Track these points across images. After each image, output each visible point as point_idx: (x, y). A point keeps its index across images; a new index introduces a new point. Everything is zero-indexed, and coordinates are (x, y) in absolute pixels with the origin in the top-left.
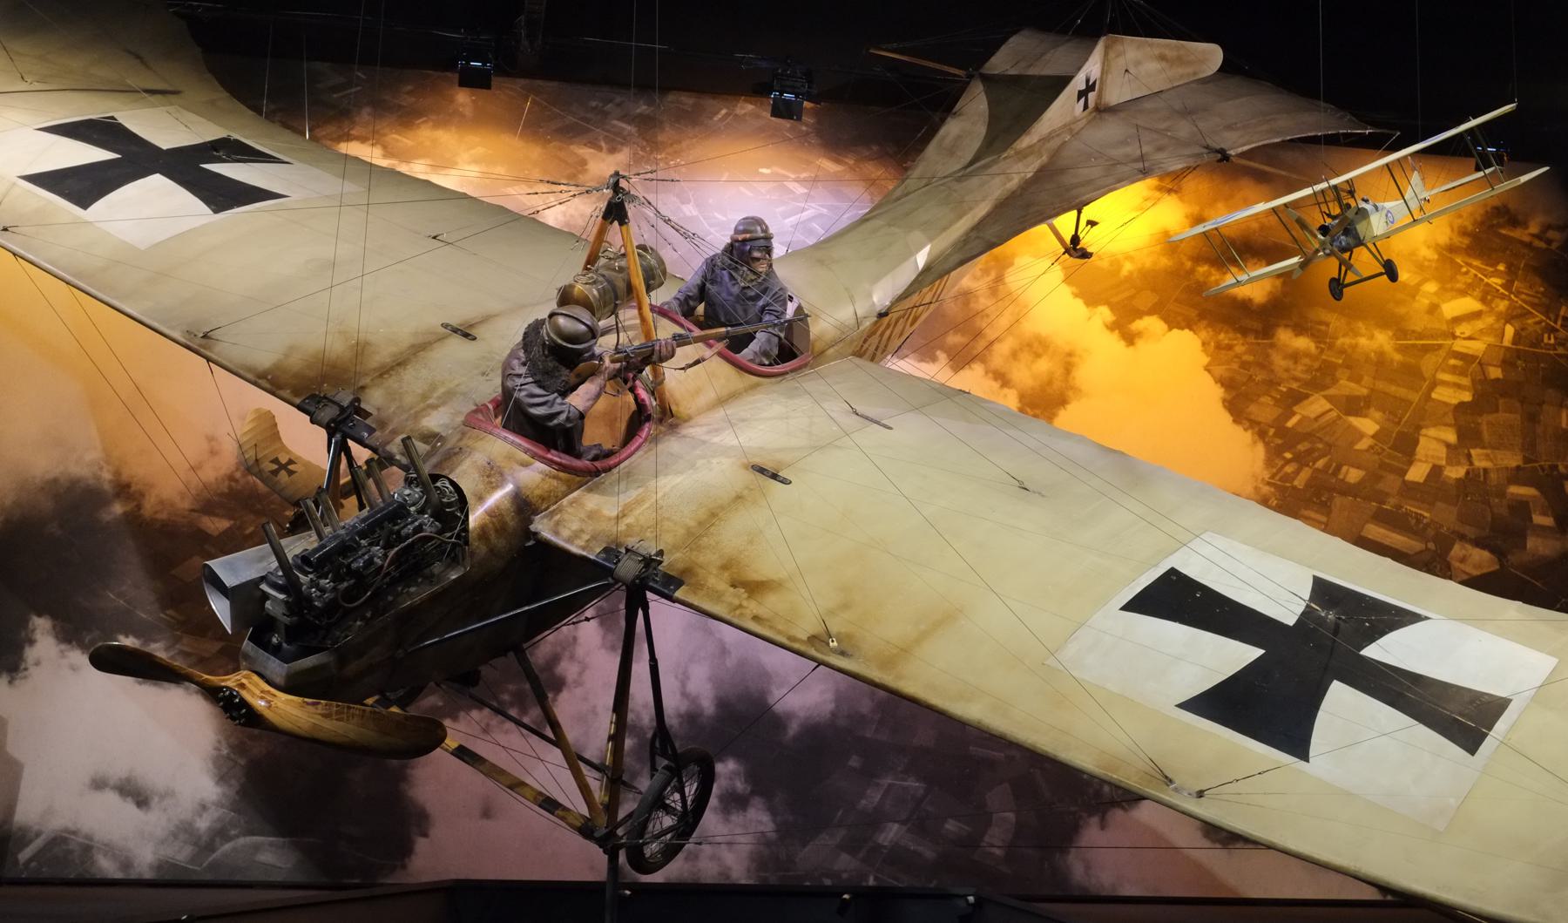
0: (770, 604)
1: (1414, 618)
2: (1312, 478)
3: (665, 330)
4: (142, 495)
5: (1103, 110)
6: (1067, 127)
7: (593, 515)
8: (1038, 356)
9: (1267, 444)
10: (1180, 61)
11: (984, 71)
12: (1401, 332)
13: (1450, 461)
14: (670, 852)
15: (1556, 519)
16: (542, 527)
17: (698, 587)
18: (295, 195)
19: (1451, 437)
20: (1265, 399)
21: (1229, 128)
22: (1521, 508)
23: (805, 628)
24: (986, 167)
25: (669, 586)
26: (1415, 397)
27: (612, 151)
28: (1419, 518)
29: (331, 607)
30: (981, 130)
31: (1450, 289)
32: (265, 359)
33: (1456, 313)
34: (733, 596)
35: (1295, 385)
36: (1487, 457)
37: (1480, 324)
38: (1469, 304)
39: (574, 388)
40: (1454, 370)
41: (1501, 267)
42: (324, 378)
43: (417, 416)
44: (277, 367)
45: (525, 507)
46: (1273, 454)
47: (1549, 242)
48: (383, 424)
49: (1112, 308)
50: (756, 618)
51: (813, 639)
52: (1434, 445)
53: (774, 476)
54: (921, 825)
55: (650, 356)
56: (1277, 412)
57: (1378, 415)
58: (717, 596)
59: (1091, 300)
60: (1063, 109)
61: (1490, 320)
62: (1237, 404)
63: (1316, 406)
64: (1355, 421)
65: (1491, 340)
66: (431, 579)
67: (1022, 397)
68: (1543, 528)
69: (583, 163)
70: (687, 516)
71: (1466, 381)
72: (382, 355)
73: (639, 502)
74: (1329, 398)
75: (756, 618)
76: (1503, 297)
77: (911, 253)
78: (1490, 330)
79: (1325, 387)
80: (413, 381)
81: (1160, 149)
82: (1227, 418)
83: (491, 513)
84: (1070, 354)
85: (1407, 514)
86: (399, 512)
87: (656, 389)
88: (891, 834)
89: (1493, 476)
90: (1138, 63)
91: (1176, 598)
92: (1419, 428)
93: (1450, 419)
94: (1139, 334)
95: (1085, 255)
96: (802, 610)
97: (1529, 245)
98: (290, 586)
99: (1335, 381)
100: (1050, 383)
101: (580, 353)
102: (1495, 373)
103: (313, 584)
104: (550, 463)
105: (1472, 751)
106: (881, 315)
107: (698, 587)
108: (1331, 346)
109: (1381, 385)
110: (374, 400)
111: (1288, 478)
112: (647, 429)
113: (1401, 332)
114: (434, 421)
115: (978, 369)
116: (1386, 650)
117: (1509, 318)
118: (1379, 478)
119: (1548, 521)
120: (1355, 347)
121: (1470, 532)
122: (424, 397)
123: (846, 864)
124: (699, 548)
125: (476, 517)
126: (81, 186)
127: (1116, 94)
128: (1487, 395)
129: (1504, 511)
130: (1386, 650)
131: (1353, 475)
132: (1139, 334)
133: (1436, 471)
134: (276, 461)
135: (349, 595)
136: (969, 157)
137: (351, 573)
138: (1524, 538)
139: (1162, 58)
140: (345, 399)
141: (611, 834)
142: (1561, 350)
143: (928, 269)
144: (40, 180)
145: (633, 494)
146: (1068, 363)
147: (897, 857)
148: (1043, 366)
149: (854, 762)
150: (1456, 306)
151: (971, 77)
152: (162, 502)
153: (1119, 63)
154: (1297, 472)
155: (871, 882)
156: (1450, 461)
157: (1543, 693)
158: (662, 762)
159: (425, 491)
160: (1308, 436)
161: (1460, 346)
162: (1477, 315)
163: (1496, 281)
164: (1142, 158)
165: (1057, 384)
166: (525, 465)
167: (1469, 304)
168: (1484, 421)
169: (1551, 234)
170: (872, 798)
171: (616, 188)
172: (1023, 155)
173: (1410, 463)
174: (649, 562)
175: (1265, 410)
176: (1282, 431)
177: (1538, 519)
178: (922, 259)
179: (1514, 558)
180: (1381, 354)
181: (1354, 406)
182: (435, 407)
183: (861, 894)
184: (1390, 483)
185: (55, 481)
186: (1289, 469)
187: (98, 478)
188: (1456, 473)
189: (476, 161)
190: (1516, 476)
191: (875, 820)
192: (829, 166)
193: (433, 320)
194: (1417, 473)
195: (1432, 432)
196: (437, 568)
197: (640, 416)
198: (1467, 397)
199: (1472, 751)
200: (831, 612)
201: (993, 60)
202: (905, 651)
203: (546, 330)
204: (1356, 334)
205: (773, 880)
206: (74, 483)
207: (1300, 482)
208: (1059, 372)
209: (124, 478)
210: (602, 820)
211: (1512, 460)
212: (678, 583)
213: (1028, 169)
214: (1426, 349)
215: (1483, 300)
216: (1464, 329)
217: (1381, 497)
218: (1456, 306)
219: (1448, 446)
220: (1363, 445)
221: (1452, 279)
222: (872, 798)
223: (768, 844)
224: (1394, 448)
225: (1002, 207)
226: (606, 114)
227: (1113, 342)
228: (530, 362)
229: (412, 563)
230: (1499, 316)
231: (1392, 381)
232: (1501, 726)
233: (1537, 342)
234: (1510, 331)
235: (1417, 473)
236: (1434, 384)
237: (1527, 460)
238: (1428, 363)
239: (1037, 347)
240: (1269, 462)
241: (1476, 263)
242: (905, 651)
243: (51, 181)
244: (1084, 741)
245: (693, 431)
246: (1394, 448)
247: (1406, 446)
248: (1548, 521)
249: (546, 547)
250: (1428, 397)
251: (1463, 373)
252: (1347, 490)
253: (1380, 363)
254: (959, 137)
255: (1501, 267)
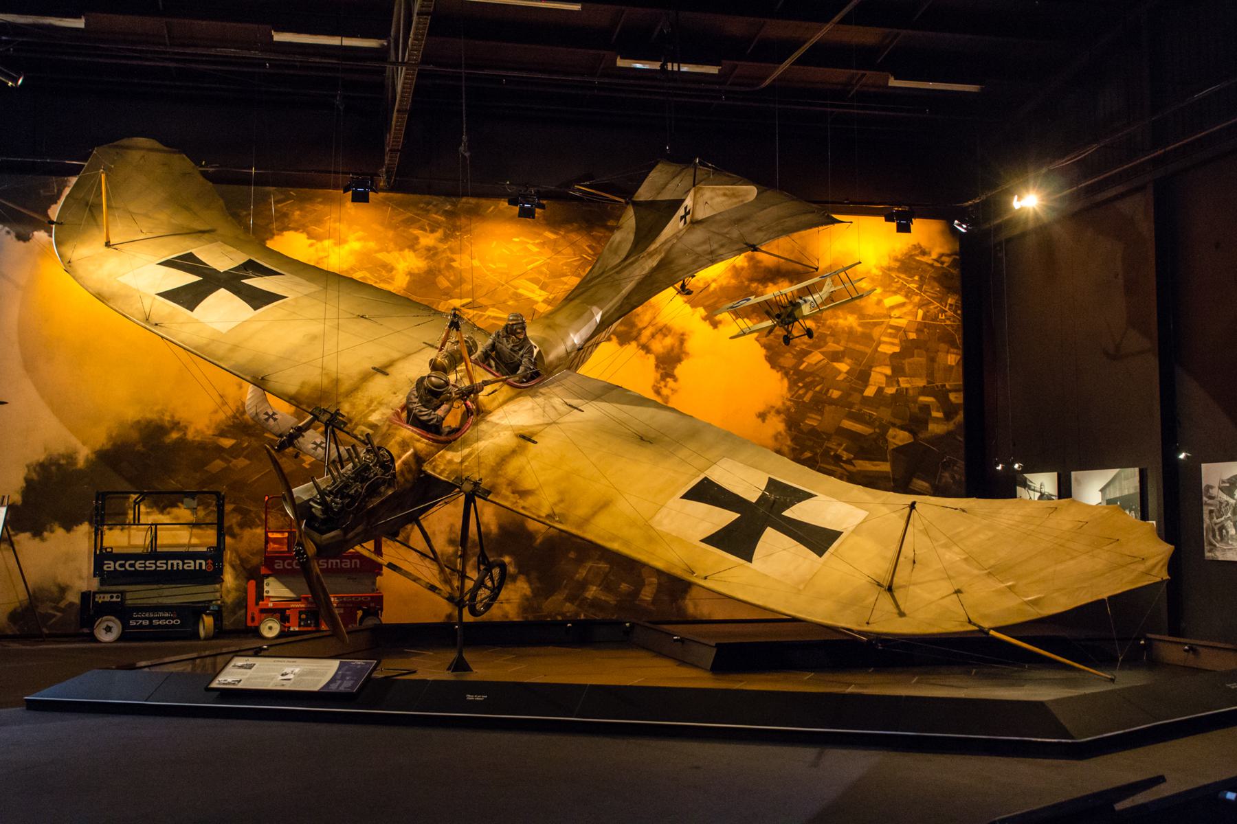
0: (530, 501)
1: (810, 496)
2: (813, 397)
3: (481, 375)
4: (186, 427)
5: (696, 223)
6: (675, 236)
7: (450, 462)
8: (665, 336)
9: (789, 379)
10: (734, 195)
11: (635, 199)
12: (862, 316)
13: (888, 385)
14: (488, 607)
15: (945, 414)
16: (427, 468)
17: (497, 494)
18: (291, 296)
19: (888, 371)
20: (788, 355)
21: (759, 229)
22: (926, 408)
23: (544, 512)
24: (632, 263)
25: (486, 494)
26: (869, 351)
27: (432, 231)
28: (871, 416)
29: (341, 509)
30: (632, 237)
31: (889, 290)
32: (292, 389)
33: (892, 304)
34: (513, 498)
35: (804, 347)
36: (908, 382)
37: (905, 310)
38: (899, 299)
39: (439, 407)
40: (890, 335)
41: (916, 278)
42: (320, 399)
43: (366, 416)
44: (298, 393)
45: (419, 459)
46: (792, 385)
47: (942, 263)
48: (350, 421)
49: (705, 308)
50: (523, 508)
51: (548, 516)
52: (879, 376)
53: (529, 440)
54: (607, 587)
55: (473, 390)
56: (794, 361)
57: (849, 361)
58: (506, 498)
59: (694, 305)
60: (674, 225)
61: (910, 307)
62: (773, 359)
63: (816, 357)
64: (837, 365)
65: (910, 318)
66: (380, 494)
67: (657, 358)
68: (937, 418)
69: (417, 238)
70: (491, 460)
71: (897, 341)
72: (344, 388)
73: (470, 455)
74: (822, 353)
75: (523, 508)
76: (917, 294)
77: (593, 316)
78: (910, 313)
79: (820, 347)
80: (361, 398)
81: (722, 246)
82: (768, 366)
83: (404, 463)
84: (683, 334)
85: (865, 414)
86: (366, 468)
87: (475, 401)
88: (592, 592)
89: (911, 392)
90: (712, 198)
91: (706, 492)
92: (871, 367)
93: (888, 361)
94: (720, 322)
95: (689, 293)
96: (544, 502)
97: (932, 265)
98: (323, 503)
99: (826, 343)
100: (672, 349)
101: (441, 393)
102: (912, 336)
103: (332, 501)
104: (429, 439)
105: (820, 555)
106: (579, 349)
107: (497, 494)
108: (824, 325)
109: (851, 345)
110: (345, 408)
111: (801, 397)
112: (472, 419)
113: (862, 316)
114: (374, 418)
115: (634, 344)
116: (795, 512)
117: (920, 306)
118: (849, 395)
119: (939, 415)
120: (836, 325)
121: (898, 422)
122: (368, 406)
123: (569, 608)
124: (497, 476)
125: (398, 463)
126: (188, 297)
127: (700, 215)
128: (908, 348)
129: (917, 410)
130: (795, 512)
131: (836, 394)
132: (720, 322)
133: (880, 390)
134: (267, 413)
135: (349, 505)
136: (623, 256)
137: (348, 496)
138: (927, 423)
139: (725, 195)
140: (333, 410)
141: (462, 600)
142: (948, 322)
143: (602, 322)
144: (167, 295)
145: (466, 451)
146: (682, 338)
147: (595, 604)
148: (669, 341)
149: (572, 555)
150: (890, 301)
151: (627, 203)
152: (197, 431)
153: (701, 201)
154: (806, 393)
155: (582, 617)
156: (888, 385)
157: (857, 530)
158: (482, 567)
159: (376, 455)
160: (811, 374)
161: (893, 322)
162: (903, 305)
163: (913, 286)
164: (712, 252)
165: (676, 351)
166: (418, 441)
167: (899, 299)
168: (907, 362)
169: (944, 259)
170: (582, 573)
171: (455, 315)
172: (651, 255)
173: (866, 386)
174: (476, 484)
175: (788, 360)
176: (797, 372)
177: (935, 414)
178: (598, 318)
179: (921, 436)
180: (851, 328)
181: (836, 357)
182: (374, 411)
183: (577, 623)
184: (856, 398)
185: (138, 422)
186: (801, 392)
187: (162, 420)
188: (890, 391)
189: (359, 239)
190: (924, 391)
191: (583, 585)
192: (550, 236)
193: (367, 365)
194: (870, 392)
195: (878, 369)
196: (382, 489)
197: (468, 412)
198: (897, 349)
199: (820, 555)
200: (555, 504)
201: (640, 190)
202: (586, 521)
203: (426, 382)
204: (838, 317)
205: (531, 618)
206: (150, 422)
207: (806, 399)
208: (677, 344)
209: (177, 419)
210: (457, 594)
211: (921, 383)
212: (489, 493)
213: (653, 262)
214: (875, 324)
215: (906, 296)
216: (896, 313)
217: (851, 405)
218: (890, 301)
219: (887, 376)
220: (840, 378)
221: (890, 285)
222: (582, 573)
223: (527, 599)
224: (857, 378)
225: (640, 284)
226: (428, 211)
227: (706, 327)
228: (420, 397)
229: (373, 490)
230: (915, 305)
231: (857, 343)
232: (835, 544)
233: (935, 318)
234: (920, 312)
235: (870, 392)
236: (879, 343)
237: (929, 382)
238: (876, 332)
239: (664, 331)
240: (790, 389)
241: (903, 276)
242: (586, 521)
243: (170, 295)
244: (663, 558)
245: (493, 418)
246: (857, 378)
247: (863, 377)
248: (939, 415)
249: (429, 476)
250: (876, 350)
251: (895, 336)
252: (833, 402)
253: (851, 332)
254: (620, 242)
255: (916, 278)
